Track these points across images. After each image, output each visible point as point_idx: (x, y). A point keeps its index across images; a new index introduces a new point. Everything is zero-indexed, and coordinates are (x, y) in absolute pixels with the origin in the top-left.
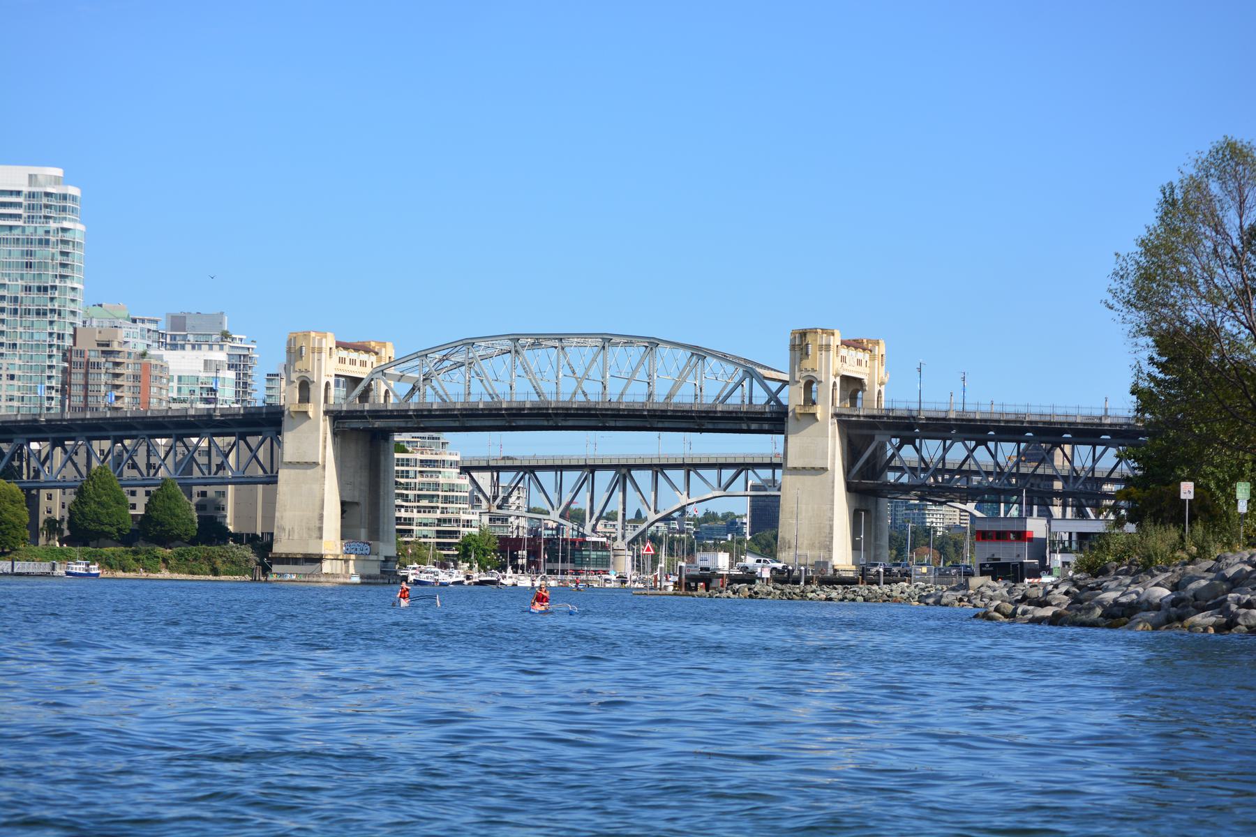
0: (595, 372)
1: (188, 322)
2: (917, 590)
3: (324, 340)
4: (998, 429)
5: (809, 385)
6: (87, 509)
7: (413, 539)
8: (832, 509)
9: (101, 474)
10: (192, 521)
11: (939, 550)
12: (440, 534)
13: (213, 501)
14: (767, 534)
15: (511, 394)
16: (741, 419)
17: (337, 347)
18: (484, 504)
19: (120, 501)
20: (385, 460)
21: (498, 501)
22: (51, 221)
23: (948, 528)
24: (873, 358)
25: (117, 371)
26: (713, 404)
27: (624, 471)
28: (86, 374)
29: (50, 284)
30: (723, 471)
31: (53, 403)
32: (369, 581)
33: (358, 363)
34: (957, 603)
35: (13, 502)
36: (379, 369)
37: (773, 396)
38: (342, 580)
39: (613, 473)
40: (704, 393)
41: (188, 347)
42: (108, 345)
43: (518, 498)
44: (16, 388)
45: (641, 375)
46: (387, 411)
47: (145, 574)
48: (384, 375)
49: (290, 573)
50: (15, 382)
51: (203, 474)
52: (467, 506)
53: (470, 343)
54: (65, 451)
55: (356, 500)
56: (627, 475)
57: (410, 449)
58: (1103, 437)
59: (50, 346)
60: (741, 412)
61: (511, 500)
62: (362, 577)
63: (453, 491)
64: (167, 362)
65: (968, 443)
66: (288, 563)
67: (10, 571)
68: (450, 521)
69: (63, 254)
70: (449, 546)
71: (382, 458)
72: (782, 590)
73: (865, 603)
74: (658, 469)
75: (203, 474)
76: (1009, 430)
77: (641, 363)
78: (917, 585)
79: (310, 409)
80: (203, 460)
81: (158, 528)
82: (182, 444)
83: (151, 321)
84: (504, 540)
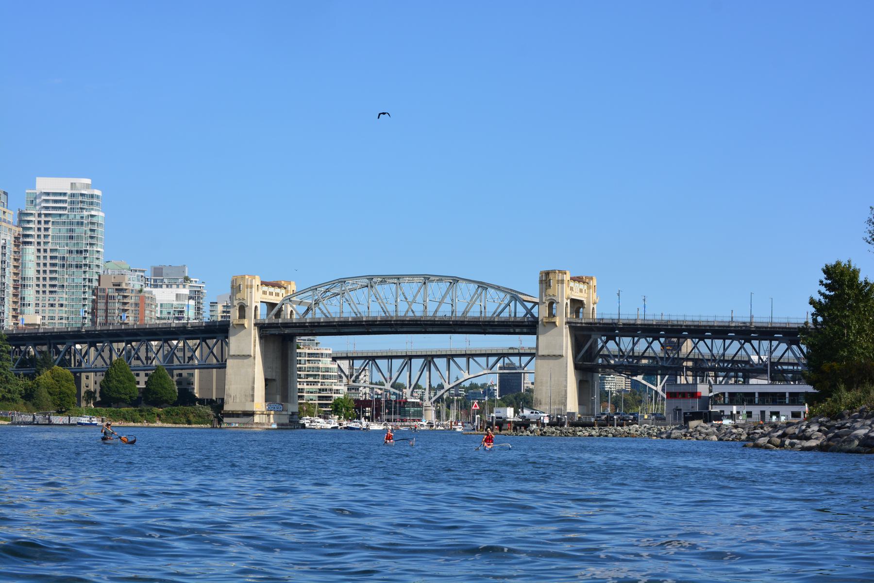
0: (419, 299)
1: (164, 271)
2: (646, 429)
3: (254, 280)
4: (667, 330)
5: (551, 304)
6: (111, 385)
7: (305, 401)
8: (566, 380)
9: (119, 363)
10: (174, 391)
11: (614, 404)
12: (320, 398)
13: (186, 379)
14: (510, 396)
15: (369, 312)
16: (510, 326)
17: (261, 285)
18: (345, 379)
19: (131, 380)
20: (291, 353)
21: (353, 378)
22: (84, 211)
23: (618, 391)
24: (589, 288)
25: (125, 301)
26: (492, 317)
27: (429, 359)
28: (107, 303)
29: (84, 249)
30: (490, 358)
31: (86, 320)
32: (283, 427)
33: (274, 294)
34: (684, 438)
35: (67, 381)
36: (287, 298)
37: (529, 311)
38: (266, 427)
39: (423, 360)
40: (487, 310)
41: (164, 286)
42: (119, 285)
43: (365, 376)
44: (64, 312)
45: (448, 300)
46: (292, 323)
47: (147, 424)
48: (291, 301)
49: (235, 423)
50: (63, 308)
51: (180, 363)
52: (336, 381)
53: (343, 281)
54: (97, 350)
55: (274, 378)
56: (432, 361)
57: (302, 347)
58: (706, 334)
59: (84, 286)
60: (510, 322)
61: (361, 377)
62: (278, 425)
63: (328, 372)
64: (154, 295)
65: (648, 339)
66: (233, 417)
67: (67, 422)
68: (326, 390)
69: (92, 230)
70: (326, 405)
71: (289, 352)
72: (561, 430)
73: (614, 438)
74: (450, 357)
75: (180, 363)
76: (650, 330)
77: (447, 292)
78: (645, 427)
79: (246, 322)
80: (180, 354)
81: (154, 396)
82: (167, 345)
83: (140, 271)
84: (357, 401)
